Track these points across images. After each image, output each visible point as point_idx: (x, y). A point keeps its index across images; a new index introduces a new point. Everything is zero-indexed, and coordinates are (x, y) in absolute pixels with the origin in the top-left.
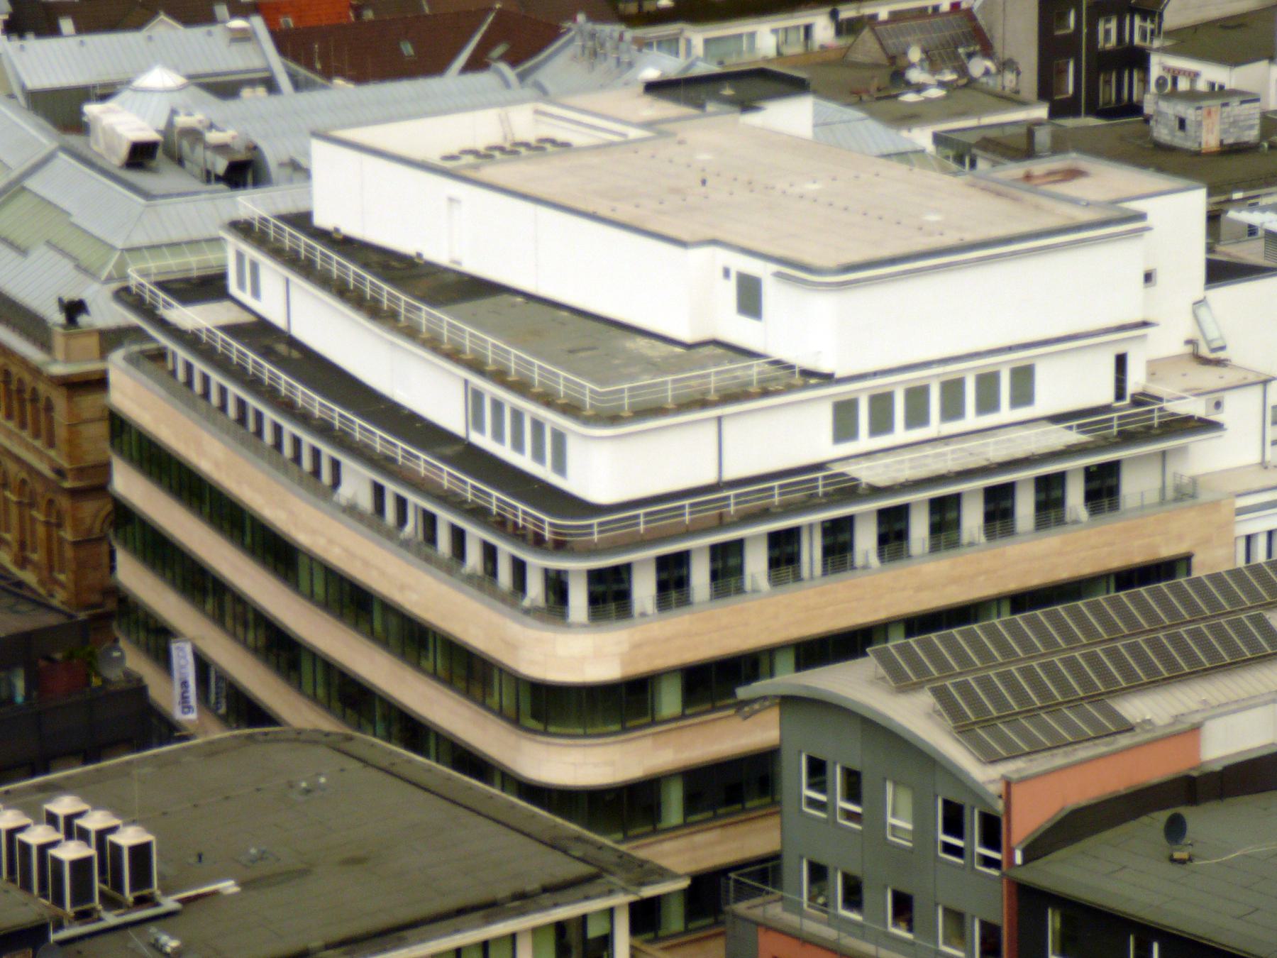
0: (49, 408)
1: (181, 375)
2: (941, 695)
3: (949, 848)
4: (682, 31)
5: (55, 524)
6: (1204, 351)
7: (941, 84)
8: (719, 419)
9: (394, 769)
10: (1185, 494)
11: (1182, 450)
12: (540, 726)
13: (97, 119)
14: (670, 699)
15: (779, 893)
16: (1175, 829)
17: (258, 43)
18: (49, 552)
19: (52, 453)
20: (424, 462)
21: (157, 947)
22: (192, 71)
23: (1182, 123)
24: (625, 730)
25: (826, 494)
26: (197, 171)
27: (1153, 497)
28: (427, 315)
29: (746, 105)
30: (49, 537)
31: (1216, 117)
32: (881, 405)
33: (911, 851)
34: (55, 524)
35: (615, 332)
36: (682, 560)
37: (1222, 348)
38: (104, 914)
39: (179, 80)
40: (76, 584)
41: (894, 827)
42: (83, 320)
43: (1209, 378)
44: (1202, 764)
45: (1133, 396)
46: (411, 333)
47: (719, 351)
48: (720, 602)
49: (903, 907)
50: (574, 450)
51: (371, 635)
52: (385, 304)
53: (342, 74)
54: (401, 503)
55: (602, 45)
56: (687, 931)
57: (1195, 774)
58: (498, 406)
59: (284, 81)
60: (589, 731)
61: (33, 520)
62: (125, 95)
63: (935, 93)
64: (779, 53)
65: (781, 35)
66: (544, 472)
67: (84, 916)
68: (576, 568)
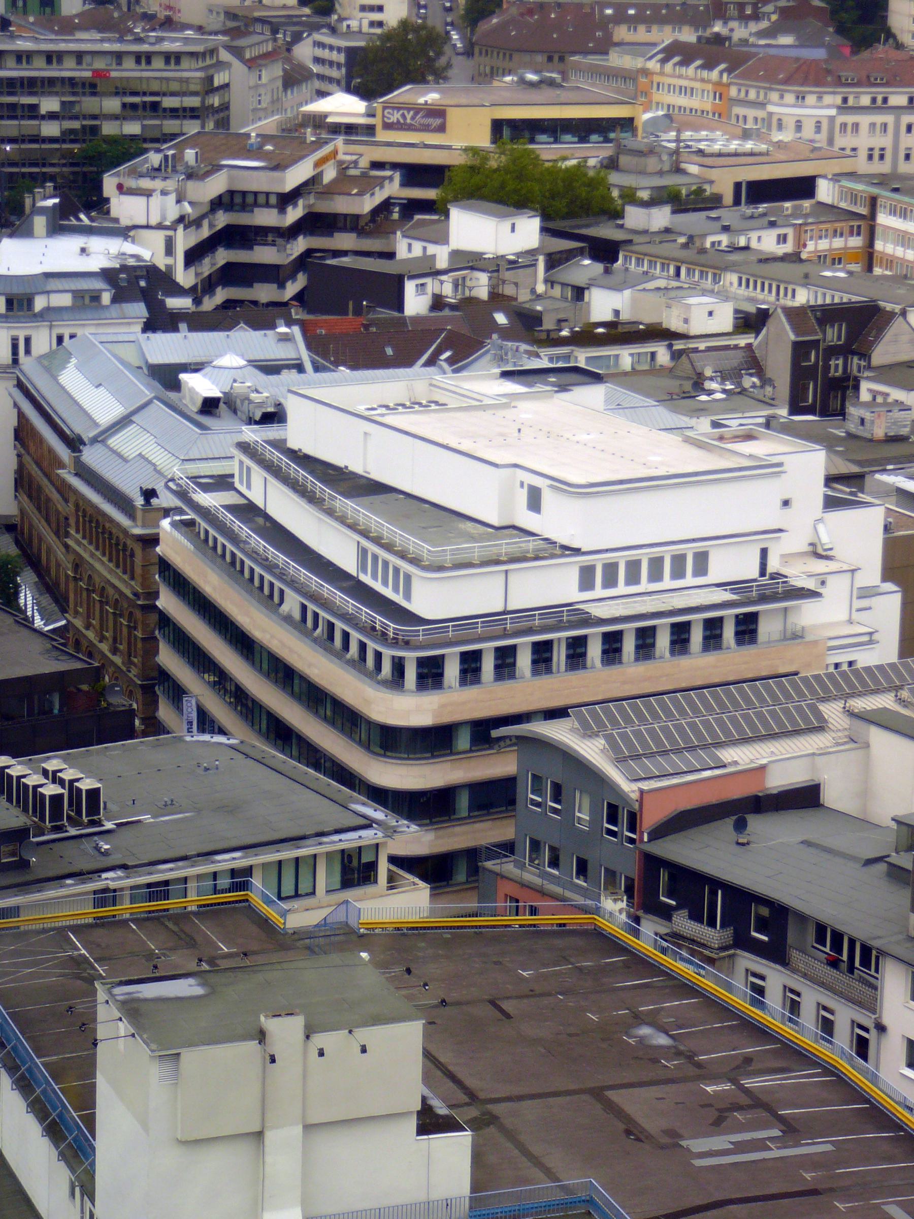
0: (132, 555)
1: (202, 536)
2: (610, 739)
4: (573, 351)
5: (132, 628)
6: (820, 551)
7: (724, 391)
8: (506, 572)
9: (264, 761)
10: (796, 636)
11: (798, 608)
12: (382, 752)
13: (186, 383)
14: (463, 741)
15: (513, 858)
16: (740, 826)
17: (295, 343)
18: (129, 643)
19: (133, 583)
20: (328, 590)
21: (97, 848)
22: (252, 358)
23: (862, 421)
24: (433, 757)
25: (568, 621)
26: (244, 418)
27: (776, 636)
29: (563, 388)
30: (130, 634)
31: (883, 419)
32: (611, 570)
33: (588, 833)
34: (132, 628)
35: (454, 517)
37: (831, 549)
38: (69, 828)
40: (143, 664)
41: (579, 818)
42: (154, 501)
43: (821, 566)
44: (767, 789)
45: (771, 574)
47: (515, 532)
48: (499, 683)
50: (416, 585)
51: (292, 694)
52: (318, 494)
53: (344, 364)
54: (316, 615)
55: (506, 354)
56: (467, 882)
57: (760, 794)
59: (308, 366)
60: (411, 756)
61: (121, 624)
62: (207, 370)
64: (633, 368)
65: (636, 358)
66: (398, 599)
68: (411, 657)
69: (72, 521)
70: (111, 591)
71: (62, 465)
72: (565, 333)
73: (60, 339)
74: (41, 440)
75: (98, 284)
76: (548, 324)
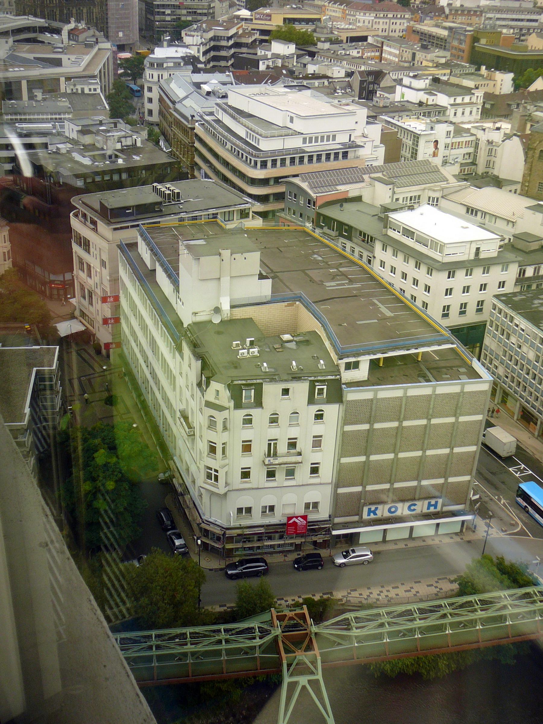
2: (309, 182)
3: (308, 207)
14: (272, 182)
20: (238, 142)
23: (377, 102)
28: (244, 120)
32: (311, 139)
36: (276, 160)
39: (217, 82)
43: (365, 139)
46: (239, 122)
49: (301, 215)
58: (250, 134)
59: (234, 83)
63: (340, 94)
66: (256, 145)
67: (170, 202)
68: (259, 160)
69: (173, 123)
70: (183, 142)
71: (171, 109)
72: (301, 76)
73: (170, 75)
74: (165, 102)
75: (180, 60)
76: (296, 74)
